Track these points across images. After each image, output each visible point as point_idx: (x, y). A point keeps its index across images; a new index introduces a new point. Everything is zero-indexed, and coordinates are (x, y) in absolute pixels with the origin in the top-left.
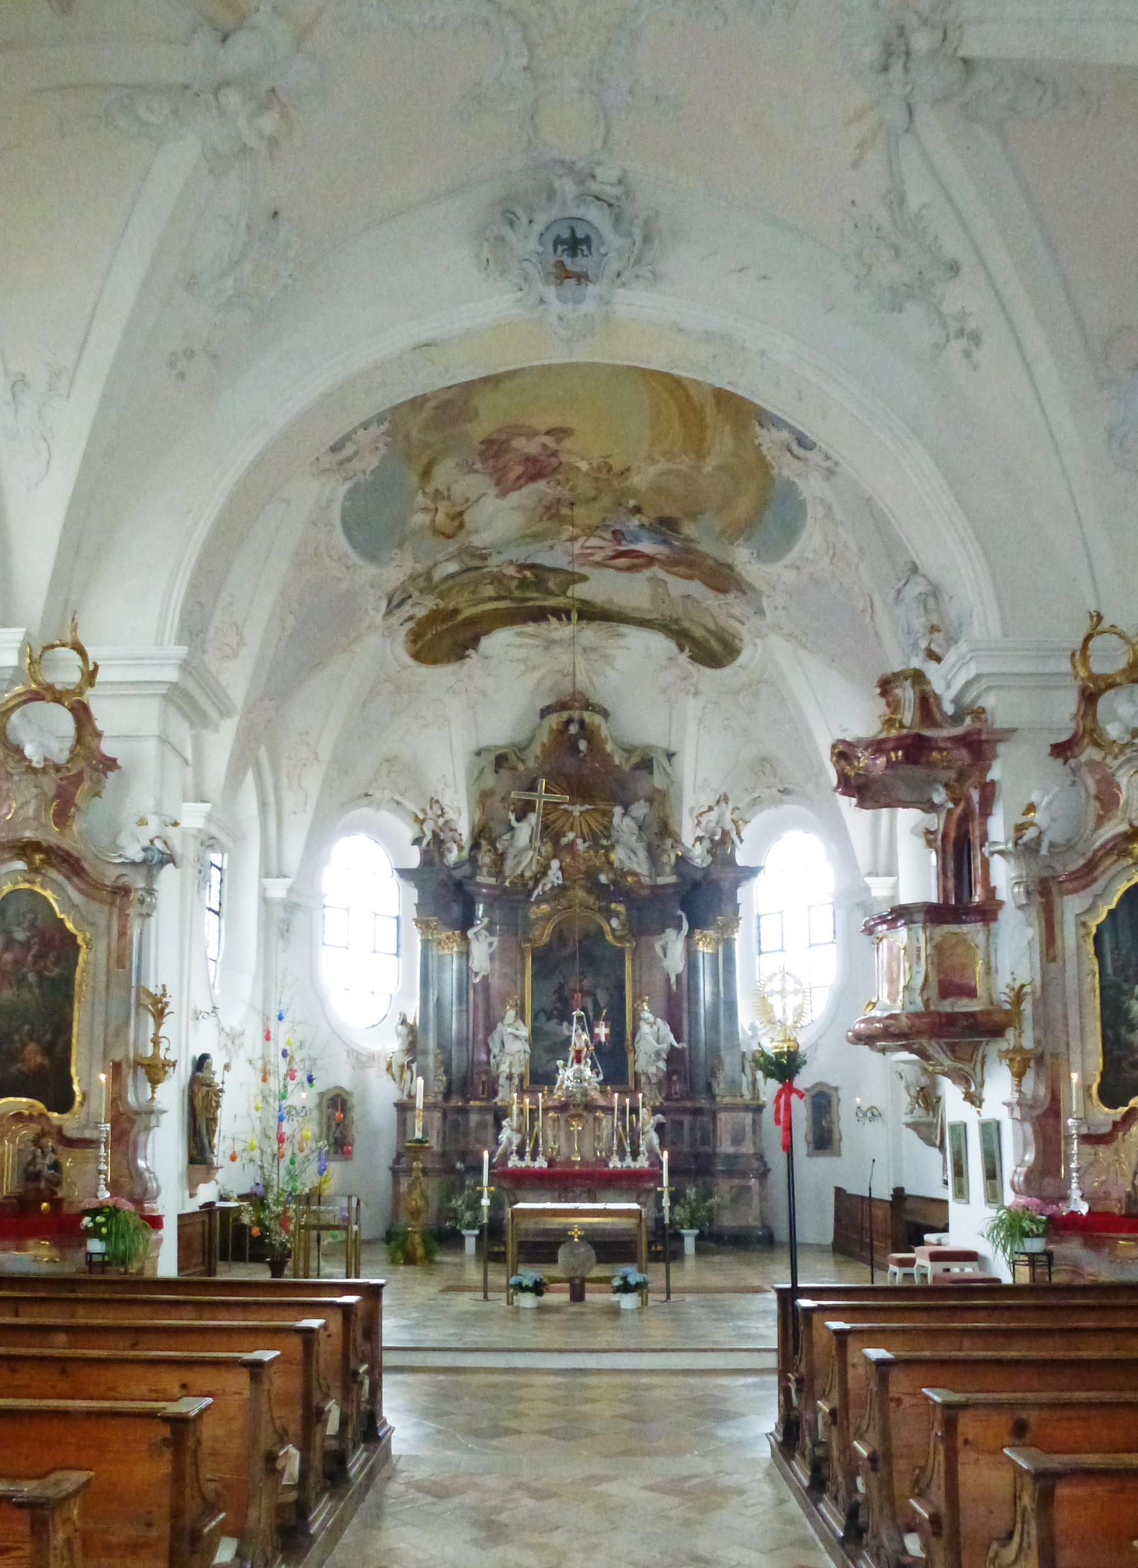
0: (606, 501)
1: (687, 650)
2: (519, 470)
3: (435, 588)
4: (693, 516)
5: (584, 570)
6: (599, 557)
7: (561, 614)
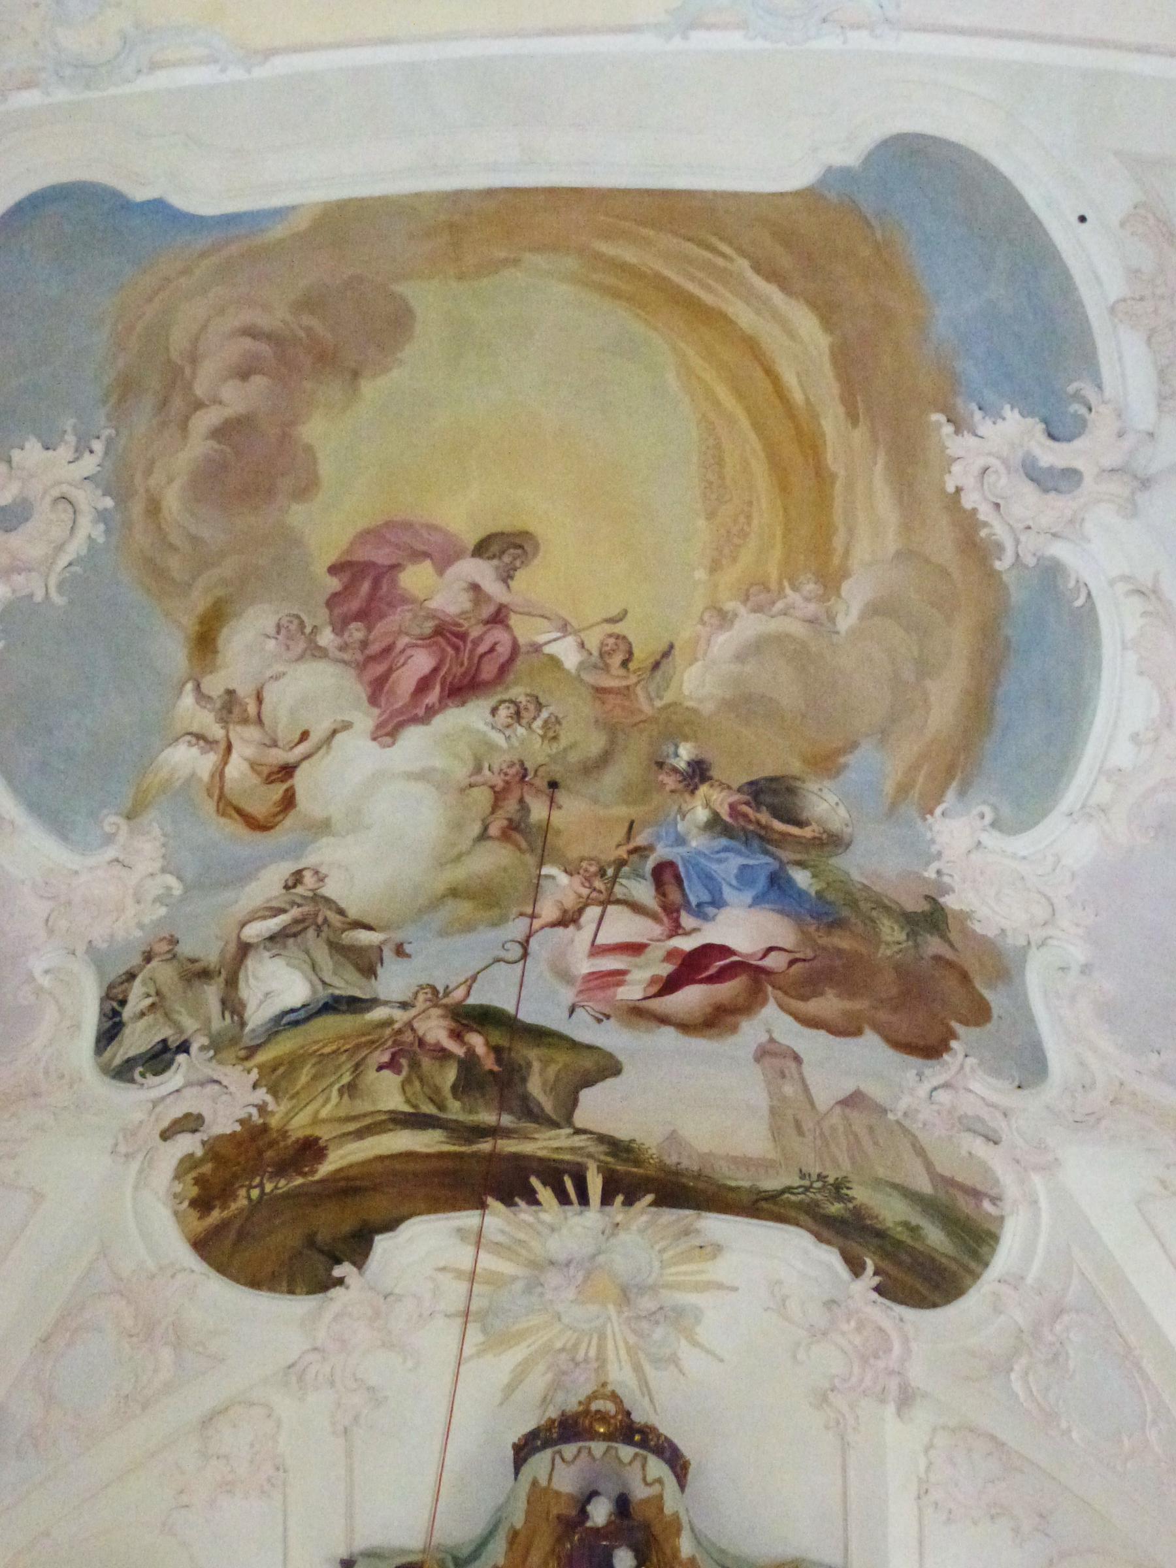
0: (627, 767)
1: (870, 1264)
2: (421, 662)
3: (252, 1051)
4: (827, 763)
5: (611, 1037)
6: (632, 992)
7: (566, 1182)
